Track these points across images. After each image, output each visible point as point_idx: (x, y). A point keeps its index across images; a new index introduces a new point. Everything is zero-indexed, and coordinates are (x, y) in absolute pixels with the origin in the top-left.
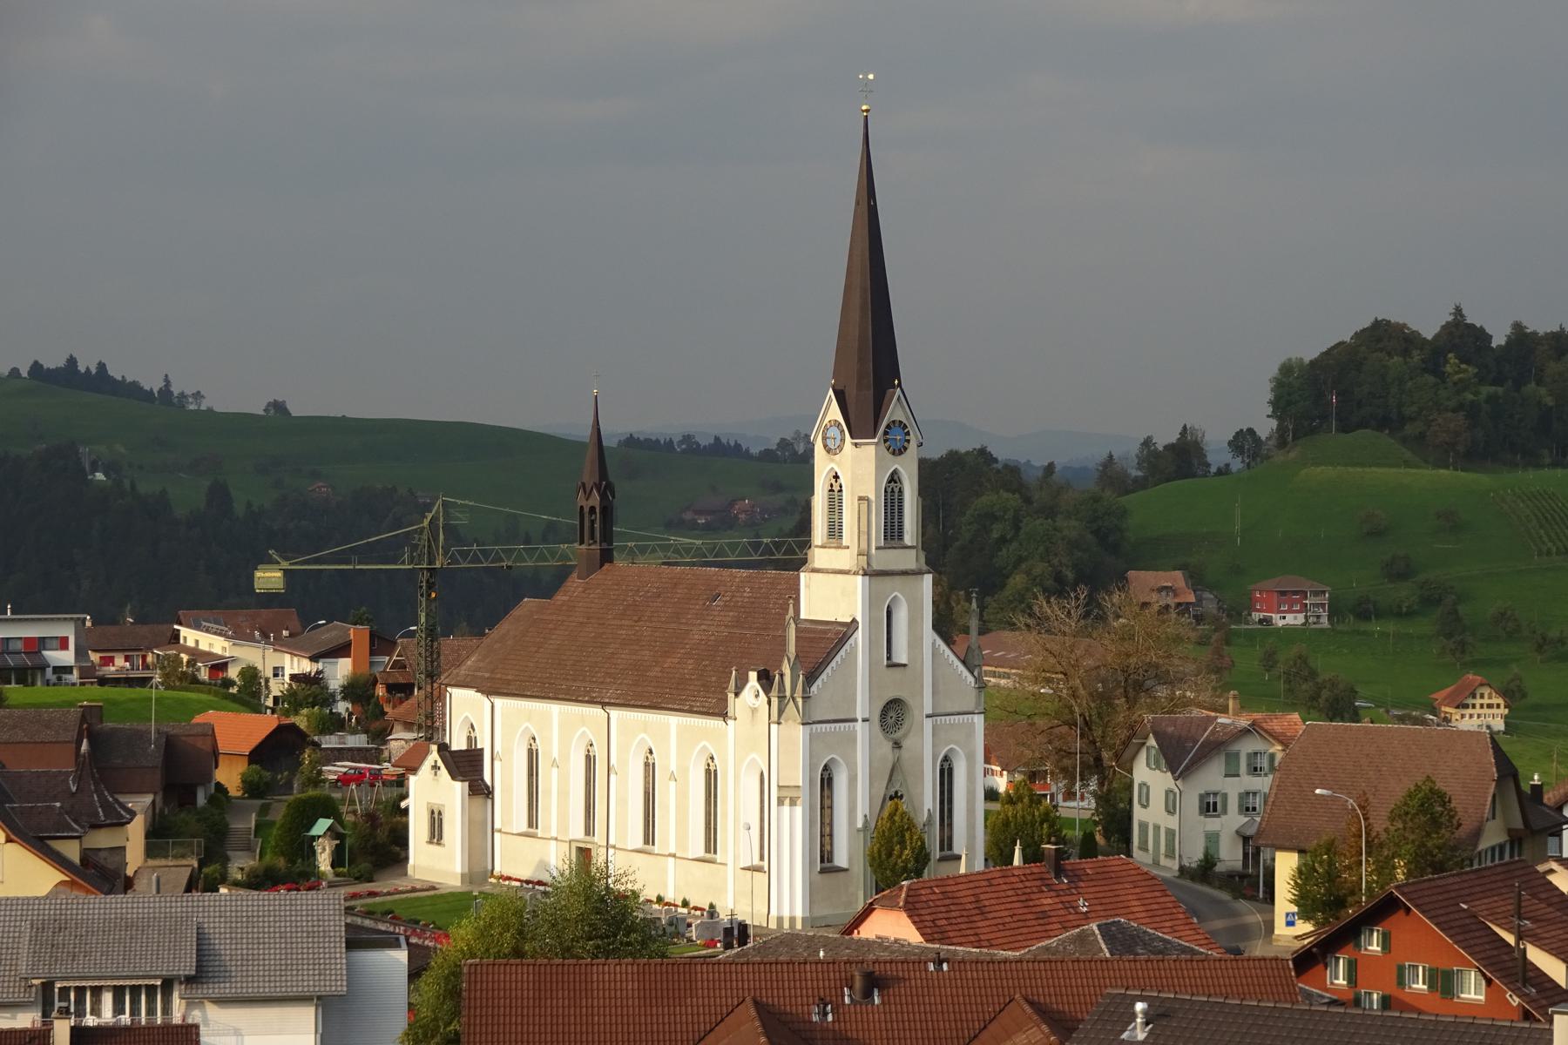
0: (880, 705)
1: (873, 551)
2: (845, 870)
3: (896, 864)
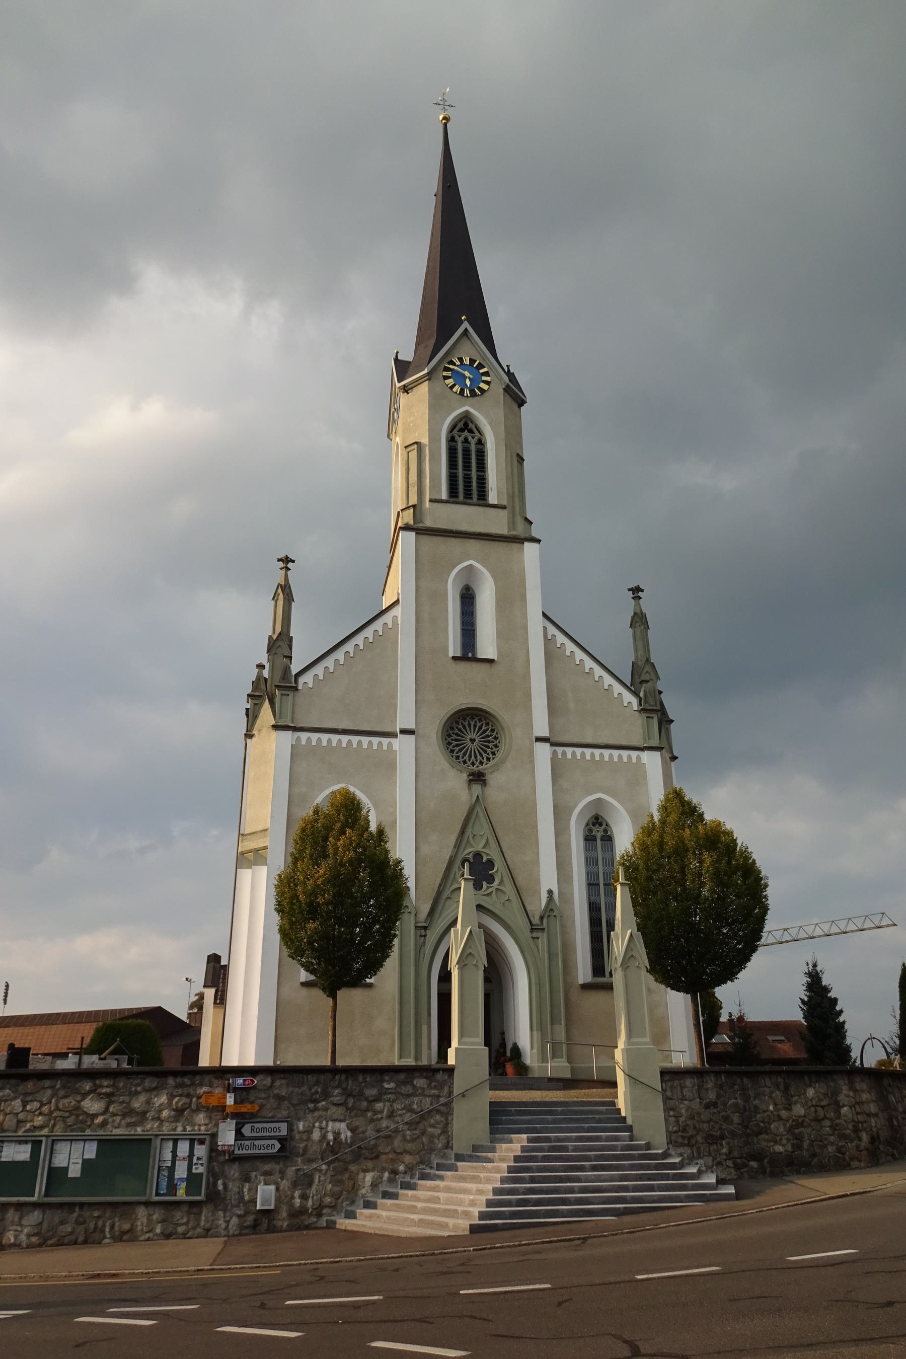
0: (443, 713)
1: (427, 504)
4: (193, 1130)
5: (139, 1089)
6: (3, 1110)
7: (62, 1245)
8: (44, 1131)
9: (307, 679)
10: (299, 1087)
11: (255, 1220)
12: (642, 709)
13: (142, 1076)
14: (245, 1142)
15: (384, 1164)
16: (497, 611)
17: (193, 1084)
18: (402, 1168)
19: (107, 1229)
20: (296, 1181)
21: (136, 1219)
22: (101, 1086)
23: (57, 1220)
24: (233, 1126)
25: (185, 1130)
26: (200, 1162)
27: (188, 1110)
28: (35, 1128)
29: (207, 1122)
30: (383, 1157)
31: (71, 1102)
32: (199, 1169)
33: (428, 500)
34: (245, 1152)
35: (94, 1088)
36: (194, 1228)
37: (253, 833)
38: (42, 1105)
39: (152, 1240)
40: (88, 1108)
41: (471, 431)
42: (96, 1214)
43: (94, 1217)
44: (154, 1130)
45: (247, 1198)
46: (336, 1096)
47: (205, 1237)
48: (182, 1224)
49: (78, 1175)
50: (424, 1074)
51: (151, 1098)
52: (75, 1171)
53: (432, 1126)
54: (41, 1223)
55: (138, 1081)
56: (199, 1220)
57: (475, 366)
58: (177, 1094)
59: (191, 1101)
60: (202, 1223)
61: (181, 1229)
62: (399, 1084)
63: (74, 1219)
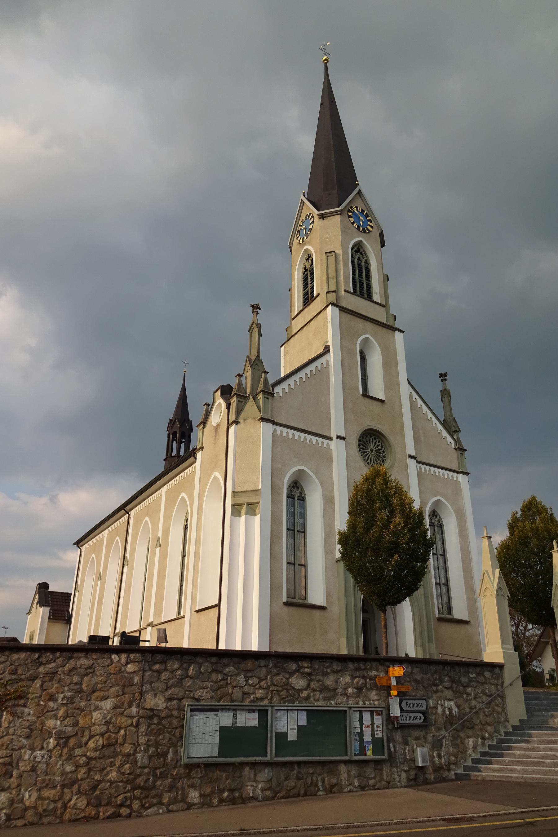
2: (323, 608)
3: (381, 537)
4: (370, 704)
5: (329, 670)
6: (231, 683)
7: (289, 797)
8: (264, 702)
9: (278, 390)
10: (426, 674)
11: (416, 774)
12: (458, 448)
13: (330, 661)
14: (404, 714)
15: (478, 733)
16: (384, 370)
17: (365, 669)
18: (487, 735)
19: (320, 783)
20: (433, 744)
21: (340, 774)
22: (303, 667)
23: (282, 776)
24: (398, 702)
25: (364, 704)
26: (379, 729)
27: (365, 688)
28: (257, 699)
29: (378, 698)
30: (476, 727)
31: (282, 679)
32: (379, 735)
33: (343, 290)
34: (405, 722)
35: (298, 669)
36: (380, 781)
37: (245, 492)
38: (261, 680)
39: (353, 792)
40: (295, 684)
41: (361, 254)
42: (311, 771)
43: (310, 773)
44: (344, 703)
45: (408, 757)
46: (446, 682)
47: (388, 788)
48: (372, 778)
49: (296, 739)
50: (489, 669)
51: (338, 678)
52: (293, 736)
53: (497, 706)
54: (271, 780)
55: (327, 664)
56: (382, 775)
57: (364, 214)
58: (356, 676)
59: (366, 681)
60: (385, 778)
61: (371, 782)
62: (479, 674)
63: (295, 775)
